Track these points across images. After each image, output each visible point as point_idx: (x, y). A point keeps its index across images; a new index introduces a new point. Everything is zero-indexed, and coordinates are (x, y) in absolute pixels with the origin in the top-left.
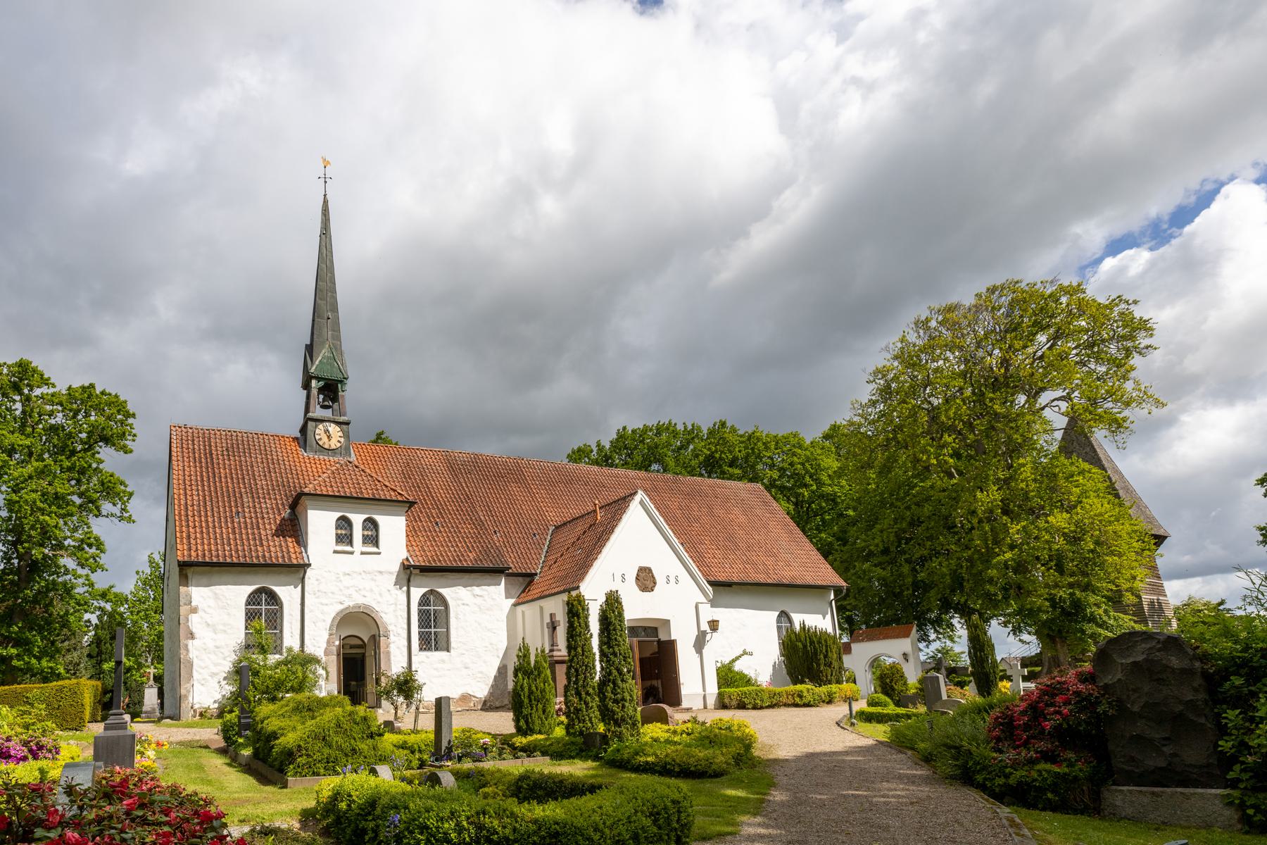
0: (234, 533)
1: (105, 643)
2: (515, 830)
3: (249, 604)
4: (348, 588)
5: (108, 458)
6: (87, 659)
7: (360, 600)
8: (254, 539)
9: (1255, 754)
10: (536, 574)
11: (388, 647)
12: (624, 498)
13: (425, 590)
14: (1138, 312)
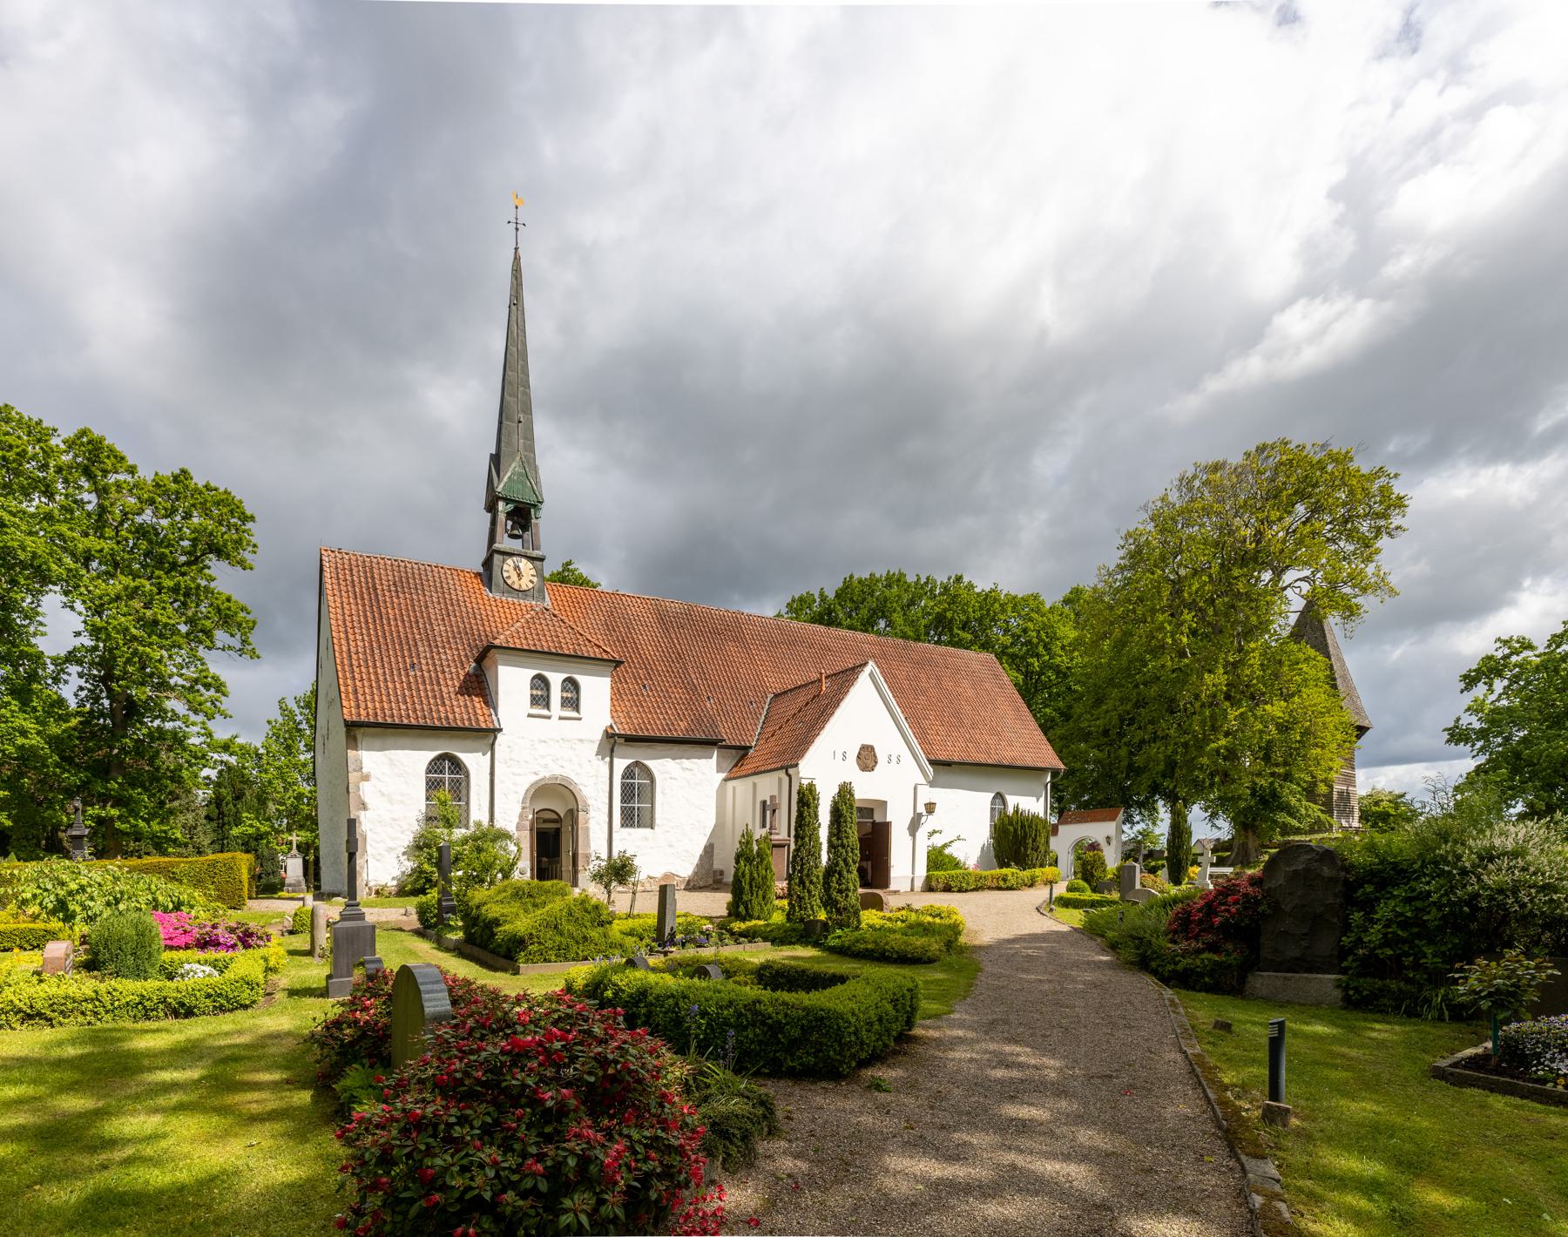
0: (410, 689)
1: (227, 804)
2: (786, 1015)
3: (430, 772)
4: (544, 757)
5: (222, 577)
6: (204, 821)
7: (557, 771)
8: (435, 697)
9: (1366, 947)
10: (751, 747)
11: (587, 822)
12: (853, 669)
13: (629, 761)
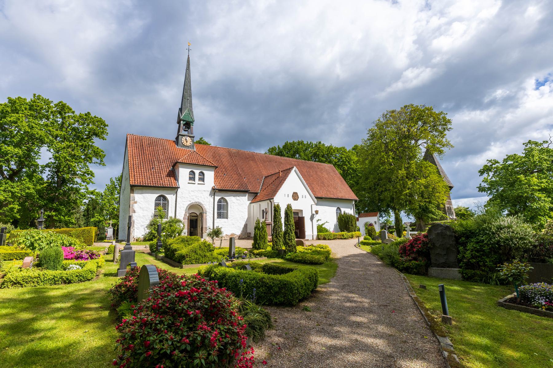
0: (152, 175)
2: (273, 283)
3: (156, 201)
4: (193, 196)
5: (97, 142)
6: (82, 216)
7: (197, 200)
8: (159, 177)
12: (289, 169)
14: (448, 117)
